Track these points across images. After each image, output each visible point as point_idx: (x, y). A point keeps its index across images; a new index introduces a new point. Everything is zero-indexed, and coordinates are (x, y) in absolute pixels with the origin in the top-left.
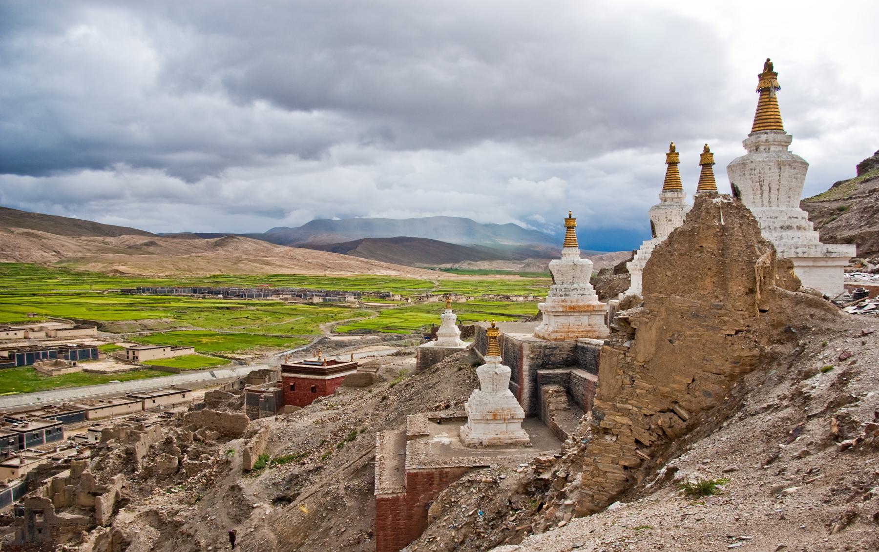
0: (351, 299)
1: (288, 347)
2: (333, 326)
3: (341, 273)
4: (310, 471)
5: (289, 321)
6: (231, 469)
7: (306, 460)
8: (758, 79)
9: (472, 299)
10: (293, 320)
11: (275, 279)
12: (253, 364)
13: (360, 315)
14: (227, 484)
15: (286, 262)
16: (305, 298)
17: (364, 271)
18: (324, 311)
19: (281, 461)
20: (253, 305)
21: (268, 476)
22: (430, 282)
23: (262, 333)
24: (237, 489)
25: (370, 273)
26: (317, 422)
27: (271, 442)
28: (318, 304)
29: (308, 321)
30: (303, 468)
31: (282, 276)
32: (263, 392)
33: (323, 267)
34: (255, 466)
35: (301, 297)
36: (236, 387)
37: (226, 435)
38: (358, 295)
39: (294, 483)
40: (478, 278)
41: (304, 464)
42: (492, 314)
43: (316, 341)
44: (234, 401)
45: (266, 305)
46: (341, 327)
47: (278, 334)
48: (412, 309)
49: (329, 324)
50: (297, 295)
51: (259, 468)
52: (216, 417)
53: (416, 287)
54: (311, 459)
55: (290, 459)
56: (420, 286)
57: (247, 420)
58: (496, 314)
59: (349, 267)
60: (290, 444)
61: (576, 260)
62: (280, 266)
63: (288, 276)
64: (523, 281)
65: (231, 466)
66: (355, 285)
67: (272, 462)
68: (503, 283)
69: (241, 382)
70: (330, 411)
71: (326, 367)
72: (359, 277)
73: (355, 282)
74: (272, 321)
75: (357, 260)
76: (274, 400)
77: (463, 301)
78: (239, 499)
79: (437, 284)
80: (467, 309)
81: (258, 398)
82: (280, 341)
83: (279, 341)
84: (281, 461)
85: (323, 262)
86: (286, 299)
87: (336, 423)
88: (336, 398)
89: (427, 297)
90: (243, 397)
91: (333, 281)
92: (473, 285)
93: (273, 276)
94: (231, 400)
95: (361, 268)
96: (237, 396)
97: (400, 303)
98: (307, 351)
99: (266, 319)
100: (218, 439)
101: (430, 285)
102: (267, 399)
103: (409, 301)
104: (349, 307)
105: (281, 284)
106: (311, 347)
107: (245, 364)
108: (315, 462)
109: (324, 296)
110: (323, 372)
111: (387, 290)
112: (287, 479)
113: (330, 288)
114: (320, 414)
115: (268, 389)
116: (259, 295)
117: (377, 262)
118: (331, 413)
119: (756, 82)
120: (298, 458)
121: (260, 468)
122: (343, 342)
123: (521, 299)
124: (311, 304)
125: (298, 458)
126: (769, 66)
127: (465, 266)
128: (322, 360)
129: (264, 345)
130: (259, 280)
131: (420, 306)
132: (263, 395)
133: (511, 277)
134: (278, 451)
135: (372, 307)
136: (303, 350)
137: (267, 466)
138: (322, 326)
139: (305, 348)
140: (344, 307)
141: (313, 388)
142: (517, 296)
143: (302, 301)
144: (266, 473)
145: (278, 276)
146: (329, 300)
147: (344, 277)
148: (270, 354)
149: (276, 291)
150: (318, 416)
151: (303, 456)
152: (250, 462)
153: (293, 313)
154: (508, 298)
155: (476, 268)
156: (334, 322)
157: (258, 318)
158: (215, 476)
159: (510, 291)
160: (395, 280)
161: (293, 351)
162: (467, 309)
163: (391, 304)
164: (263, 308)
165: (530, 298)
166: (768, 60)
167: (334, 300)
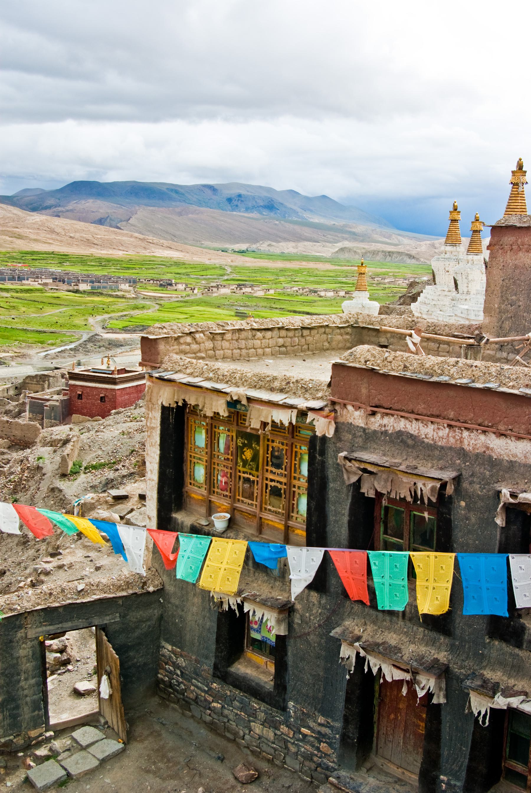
0: (125, 286)
1: (53, 344)
2: (104, 321)
3: (111, 252)
4: (124, 476)
5: (51, 312)
6: (44, 475)
7: (120, 467)
8: (511, 174)
9: (272, 292)
10: (56, 311)
11: (29, 257)
12: (13, 363)
13: (136, 308)
14: (44, 487)
15: (43, 235)
16: (69, 284)
17: (139, 250)
18: (93, 302)
19: (95, 467)
20: (7, 290)
21: (85, 480)
22: (221, 268)
23: (20, 326)
24: (56, 491)
25: (147, 253)
26: (123, 433)
27: (82, 449)
28: (84, 292)
29: (74, 313)
30: (117, 474)
31: (38, 253)
32: (48, 400)
33: (89, 243)
34: (71, 471)
35: (64, 282)
36: (12, 392)
37: (16, 444)
38: (133, 282)
39: (110, 486)
40: (280, 265)
41: (118, 470)
42: (295, 312)
43: (85, 337)
44: (12, 408)
45: (22, 291)
46: (115, 322)
47: (40, 329)
48: (198, 303)
49: (99, 318)
50: (58, 279)
51: (75, 473)
52: (6, 425)
53: (204, 273)
54: (123, 466)
55: (102, 466)
56: (209, 272)
57: (39, 430)
58: (300, 312)
59: (121, 245)
60: (100, 452)
61: (364, 302)
62: (36, 240)
63: (46, 253)
64: (334, 271)
65: (44, 471)
66: (128, 268)
67: (86, 468)
68: (310, 273)
69: (16, 388)
70: (133, 423)
71: (117, 376)
72: (134, 258)
73: (128, 264)
74: (32, 313)
75: (131, 236)
76: (60, 409)
77: (260, 294)
78: (61, 499)
79: (229, 270)
80: (265, 304)
81: (42, 406)
82: (43, 336)
83: (42, 337)
84: (95, 467)
85: (89, 237)
86: (46, 284)
87: (143, 434)
88: (138, 411)
89: (217, 287)
90: (24, 404)
91: (102, 262)
92: (273, 273)
93: (27, 253)
94: (8, 407)
95: (135, 247)
96: (15, 403)
97: (184, 294)
98: (75, 350)
99: (23, 309)
100: (9, 448)
101: (221, 272)
102: (53, 408)
103: (196, 291)
104: (123, 297)
105: (37, 263)
106: (80, 345)
107: (4, 363)
108: (128, 469)
109: (92, 282)
110: (113, 382)
111: (168, 276)
112: (103, 483)
113: (99, 272)
114: (124, 425)
115: (53, 395)
116: (12, 279)
117: (156, 240)
118: (134, 425)
119: (509, 177)
120: (111, 465)
121: (75, 473)
122: (118, 340)
123: (331, 294)
124: (77, 291)
125: (111, 465)
126: (520, 167)
127: (264, 246)
128: (112, 368)
129: (24, 341)
130: (9, 258)
131: (207, 299)
132: (48, 403)
133: (321, 266)
134: (89, 459)
135: (151, 298)
136: (71, 349)
137: (82, 472)
138: (91, 320)
139: (72, 346)
140: (117, 297)
141: (102, 398)
142: (326, 290)
143: (66, 287)
144: (82, 478)
145: (32, 253)
146: (99, 288)
147: (115, 257)
148: (32, 352)
149: (33, 273)
150: (124, 427)
151: (114, 463)
152: (67, 467)
153: (56, 302)
154: (315, 292)
155: (278, 251)
156: (106, 316)
157: (14, 307)
158: (28, 481)
159: (318, 283)
160: (177, 264)
161: (60, 349)
162: (265, 304)
163: (174, 294)
164: (19, 295)
165: (342, 294)
166: (520, 160)
167: (105, 287)
